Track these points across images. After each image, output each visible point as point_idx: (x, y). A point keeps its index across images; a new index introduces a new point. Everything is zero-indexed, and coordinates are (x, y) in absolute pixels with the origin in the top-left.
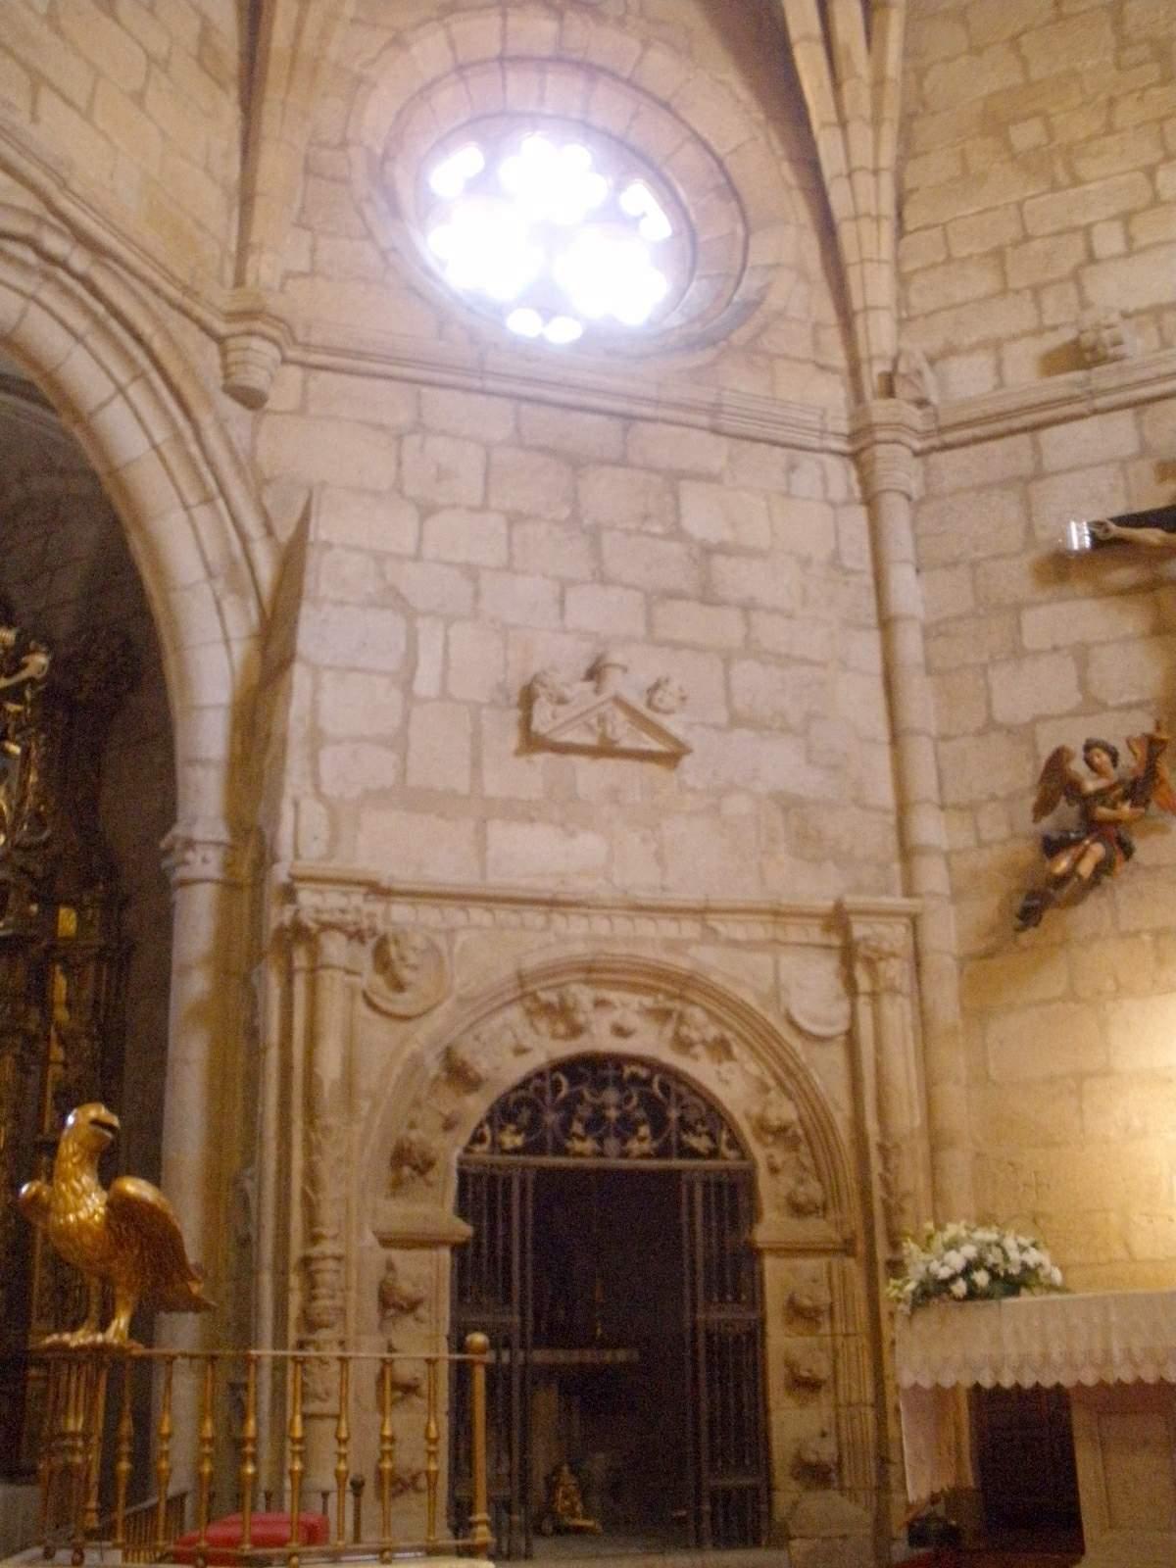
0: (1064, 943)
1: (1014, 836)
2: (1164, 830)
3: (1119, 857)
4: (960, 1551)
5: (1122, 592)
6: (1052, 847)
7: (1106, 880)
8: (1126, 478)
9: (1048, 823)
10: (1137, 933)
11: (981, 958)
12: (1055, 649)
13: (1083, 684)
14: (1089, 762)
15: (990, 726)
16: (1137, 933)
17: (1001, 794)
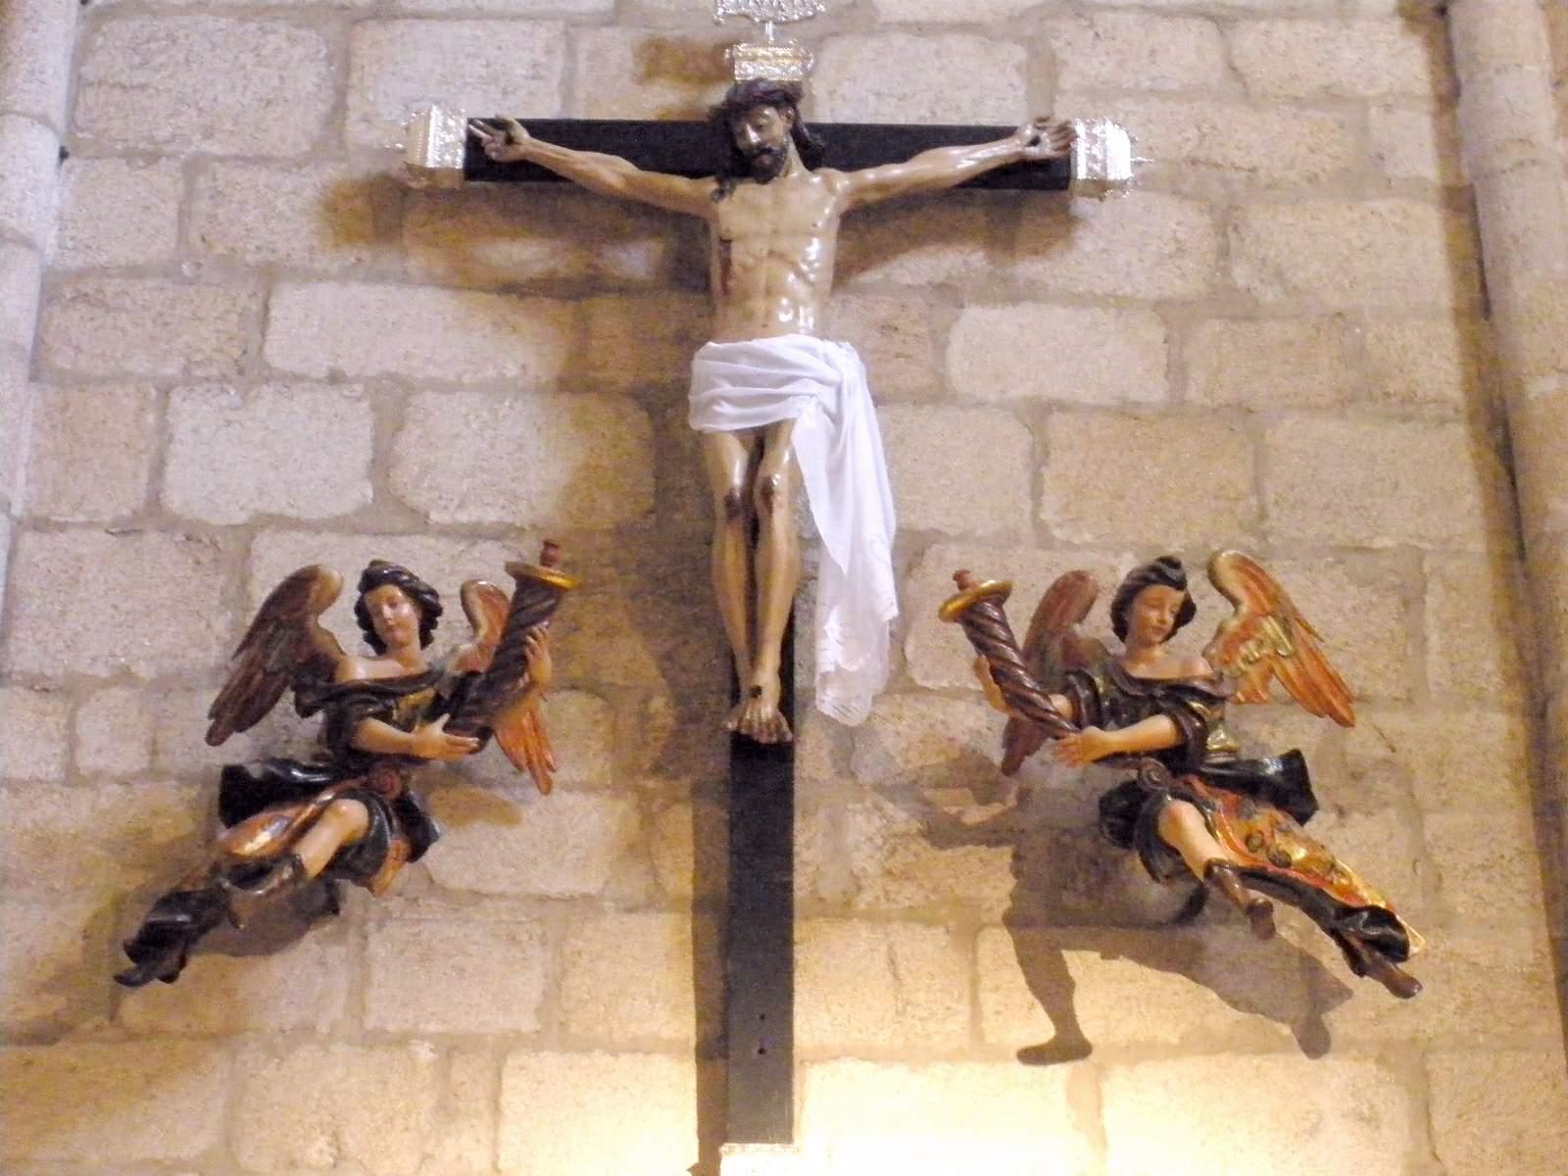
0: (226, 1037)
1: (154, 773)
2: (507, 815)
3: (396, 844)
4: (276, 468)
5: (510, 288)
6: (240, 796)
7: (353, 893)
8: (571, 53)
9: (240, 749)
10: (403, 1040)
11: (19, 1042)
12: (335, 378)
13: (381, 465)
14: (365, 616)
15: (152, 515)
16: (403, 1040)
17: (144, 671)
